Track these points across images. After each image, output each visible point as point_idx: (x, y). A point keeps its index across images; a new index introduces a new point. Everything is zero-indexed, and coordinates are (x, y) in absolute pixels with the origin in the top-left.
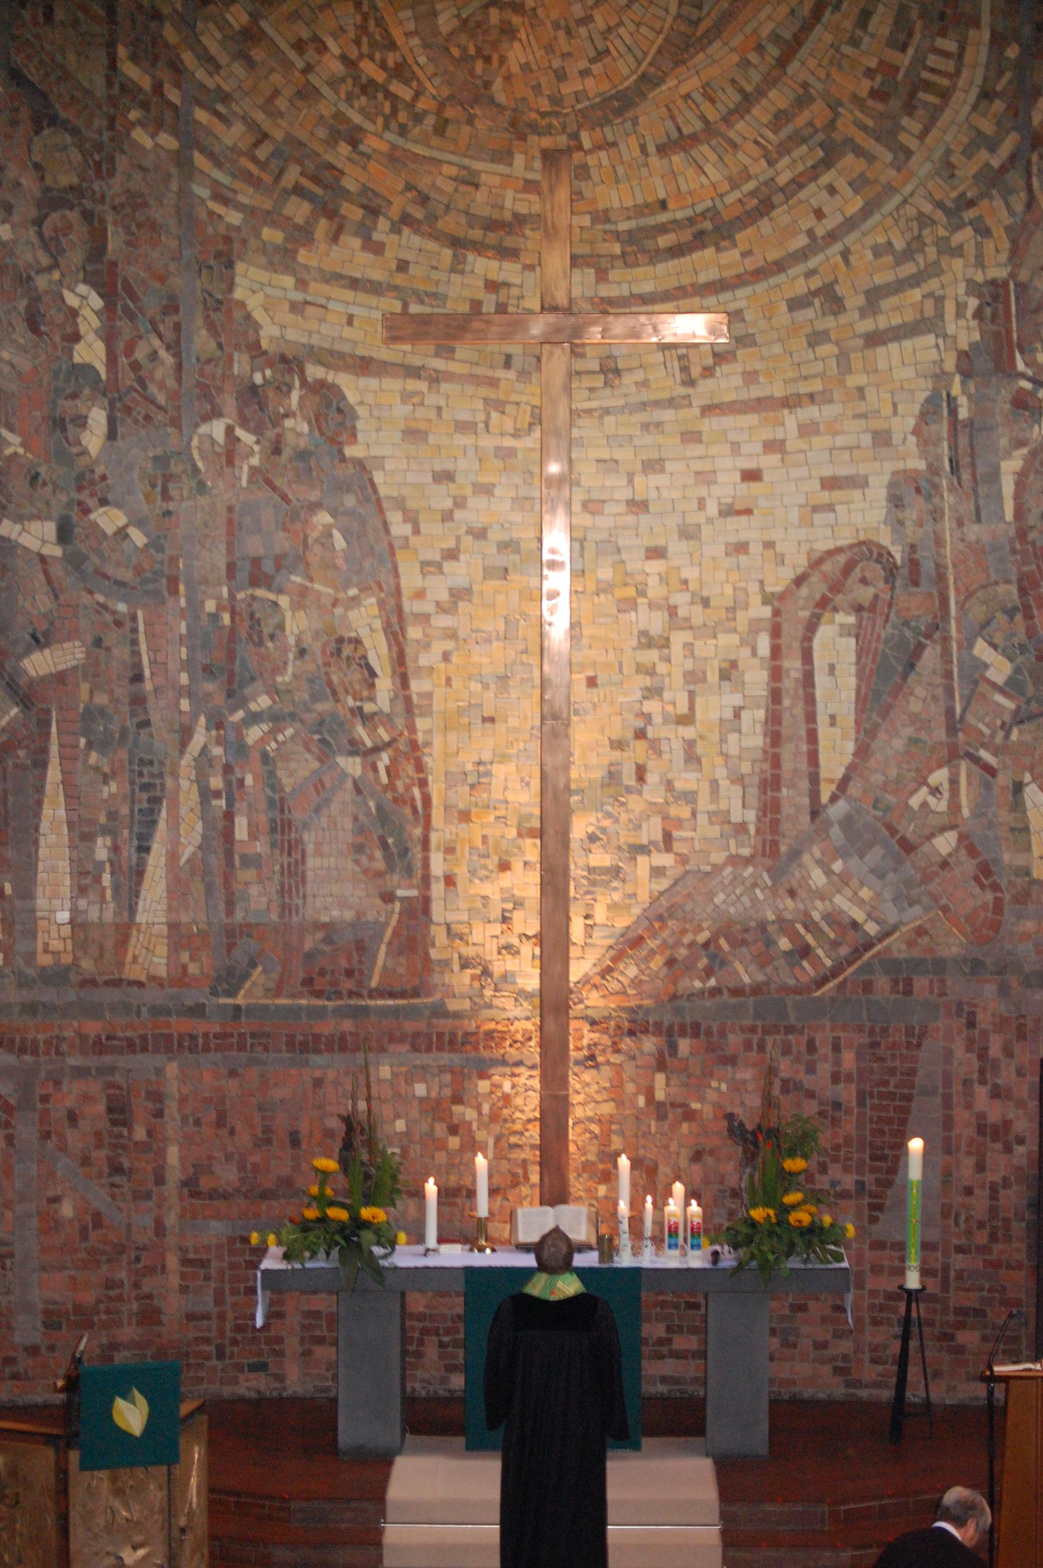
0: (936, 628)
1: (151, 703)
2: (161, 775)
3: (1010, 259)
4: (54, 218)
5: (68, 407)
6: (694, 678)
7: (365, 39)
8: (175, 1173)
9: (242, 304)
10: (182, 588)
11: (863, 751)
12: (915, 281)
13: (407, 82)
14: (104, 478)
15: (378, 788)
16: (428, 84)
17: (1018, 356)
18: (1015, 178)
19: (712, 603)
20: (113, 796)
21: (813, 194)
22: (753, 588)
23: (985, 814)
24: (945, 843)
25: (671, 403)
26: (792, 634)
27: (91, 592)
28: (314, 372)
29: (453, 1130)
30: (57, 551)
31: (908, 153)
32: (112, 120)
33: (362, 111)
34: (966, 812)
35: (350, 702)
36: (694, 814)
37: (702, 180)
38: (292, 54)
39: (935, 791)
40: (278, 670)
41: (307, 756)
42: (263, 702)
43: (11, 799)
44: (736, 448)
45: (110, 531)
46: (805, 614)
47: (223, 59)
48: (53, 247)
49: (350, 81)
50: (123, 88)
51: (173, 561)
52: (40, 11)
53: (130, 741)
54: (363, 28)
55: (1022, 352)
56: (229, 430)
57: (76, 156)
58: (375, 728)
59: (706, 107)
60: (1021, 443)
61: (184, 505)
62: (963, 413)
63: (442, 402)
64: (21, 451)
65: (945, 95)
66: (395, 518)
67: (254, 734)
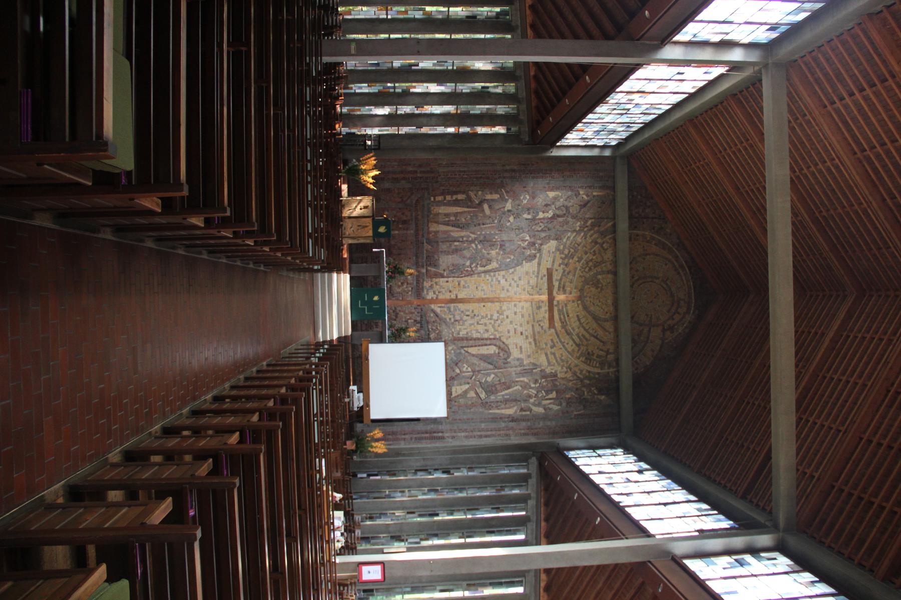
0: (496, 367)
4: (564, 209)
5: (531, 211)
6: (486, 325)
11: (473, 355)
21: (571, 342)
24: (458, 371)
28: (538, 255)
29: (402, 283)
37: (573, 324)
48: (558, 209)
67: (473, 245)
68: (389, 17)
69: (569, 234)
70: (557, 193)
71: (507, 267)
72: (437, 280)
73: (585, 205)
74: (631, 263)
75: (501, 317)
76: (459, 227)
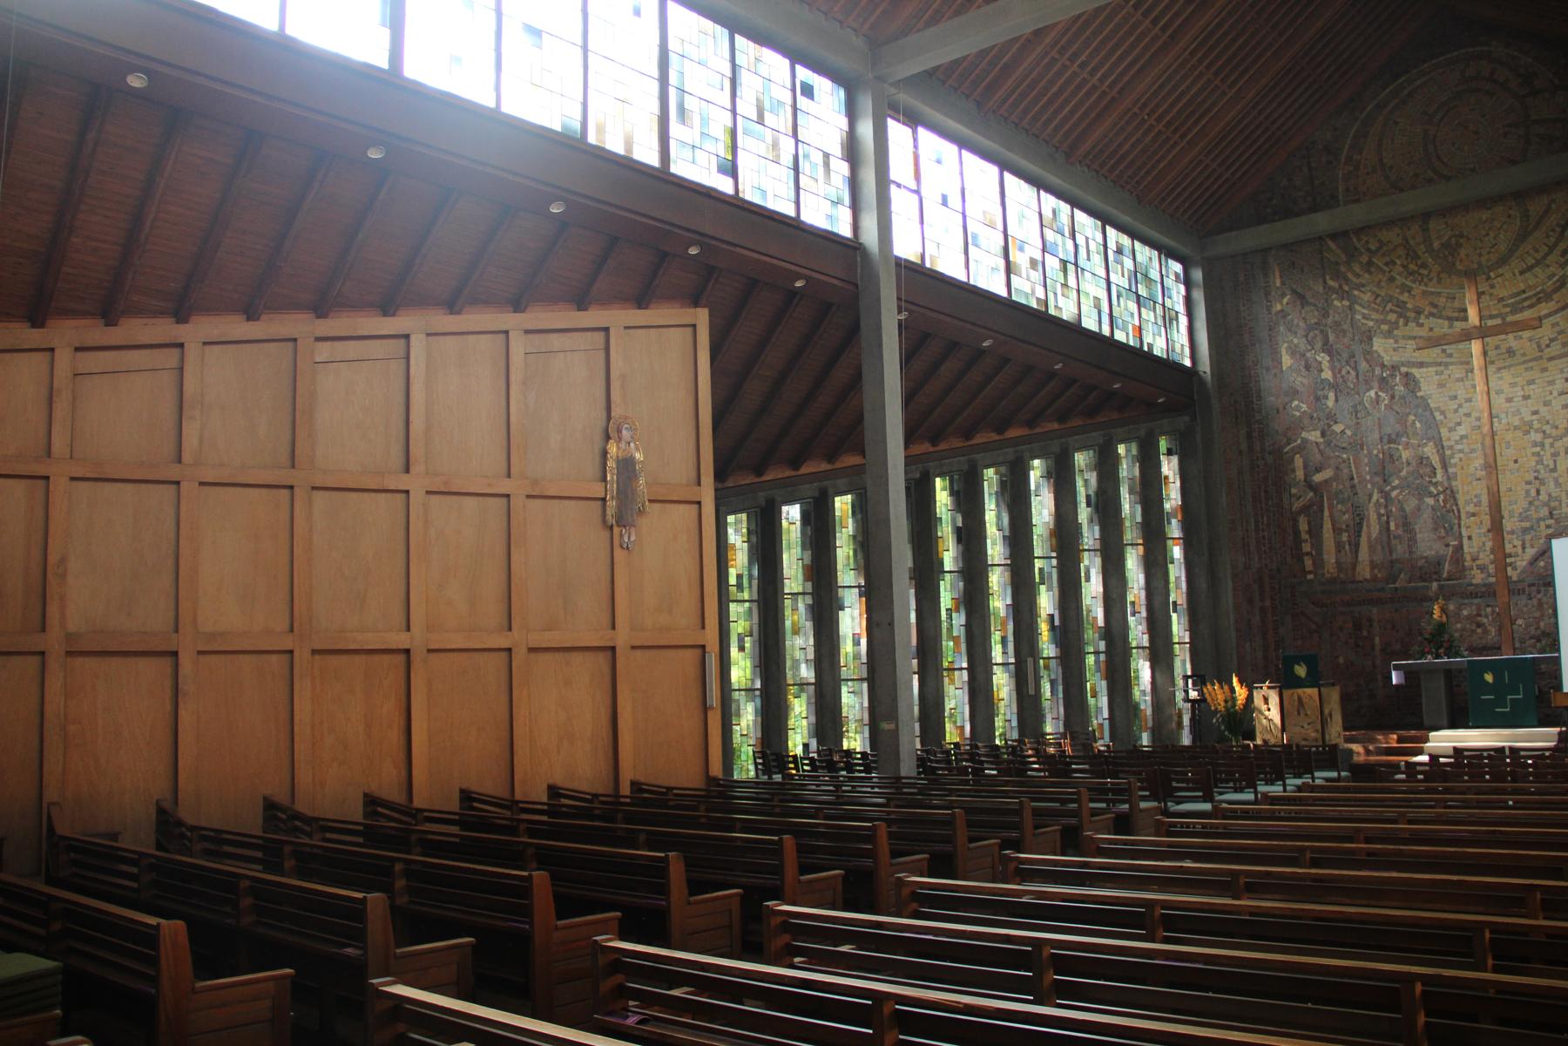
6: (1555, 455)
8: (1378, 648)
25: (1535, 359)
28: (1404, 369)
67: (1394, 494)
68: (965, 665)
69: (1358, 317)
70: (1284, 352)
71: (1432, 427)
72: (1468, 558)
73: (1302, 297)
74: (1402, 190)
75: (1536, 425)
76: (1360, 525)
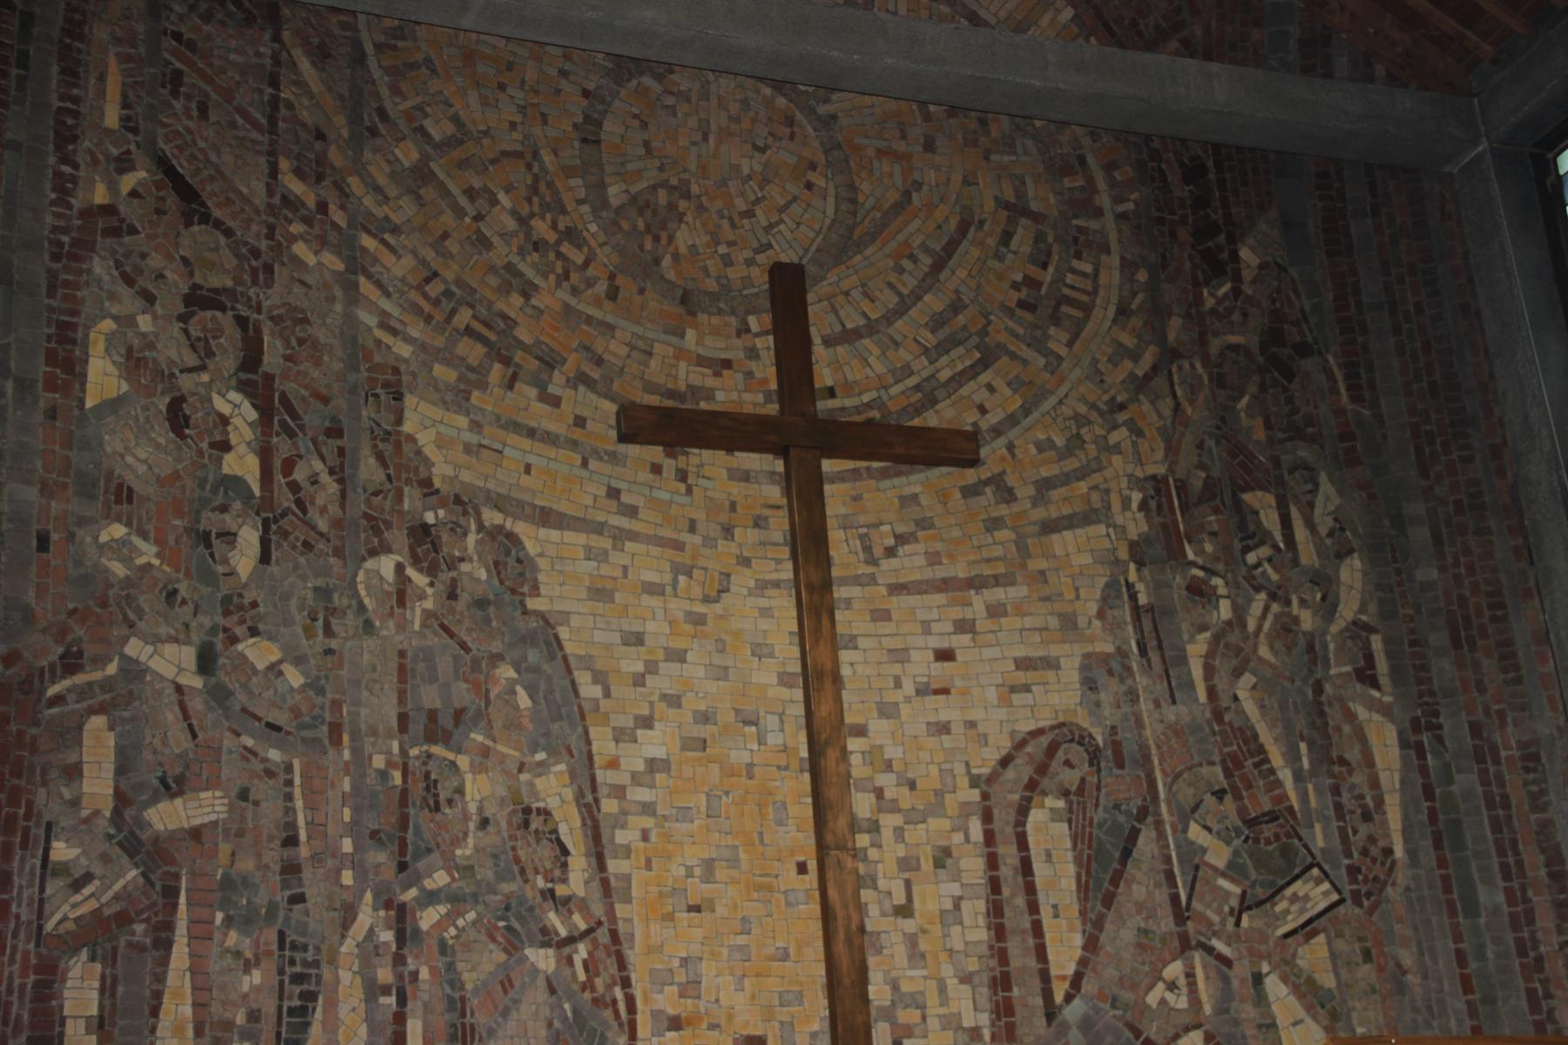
1: (307, 874)
2: (316, 964)
3: (1166, 457)
5: (211, 521)
6: (907, 864)
7: (535, 199)
9: (411, 439)
10: (346, 738)
11: (1091, 944)
12: (1081, 474)
13: (579, 247)
14: (254, 605)
15: (575, 987)
16: (598, 251)
17: (570, 1015)
18: (1159, 382)
19: (919, 786)
20: (257, 989)
21: (973, 390)
22: (960, 769)
23: (1227, 1011)
26: (1003, 820)
27: (238, 735)
28: (491, 517)
30: (197, 682)
31: (1060, 359)
32: (272, 229)
33: (535, 266)
34: (1208, 1009)
35: (540, 883)
36: (924, 1018)
38: (463, 201)
39: (1172, 986)
40: (458, 841)
41: (492, 946)
42: (440, 879)
43: (120, 990)
44: (926, 628)
45: (260, 666)
46: (1016, 797)
47: (392, 192)
48: (203, 350)
49: (522, 236)
50: (284, 198)
51: (336, 705)
52: (194, 105)
53: (280, 921)
54: (534, 189)
55: (1190, 542)
56: (400, 568)
57: (230, 262)
58: (571, 913)
59: (866, 306)
60: (1203, 628)
61: (348, 644)
62: (1143, 599)
63: (627, 562)
64: (156, 562)
65: (1087, 309)
66: (583, 678)
69: (369, 319)
70: (97, 347)
